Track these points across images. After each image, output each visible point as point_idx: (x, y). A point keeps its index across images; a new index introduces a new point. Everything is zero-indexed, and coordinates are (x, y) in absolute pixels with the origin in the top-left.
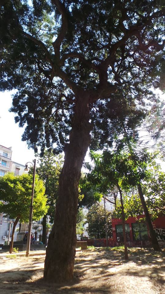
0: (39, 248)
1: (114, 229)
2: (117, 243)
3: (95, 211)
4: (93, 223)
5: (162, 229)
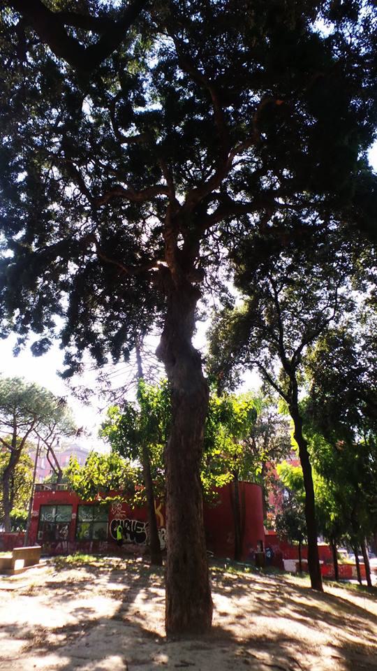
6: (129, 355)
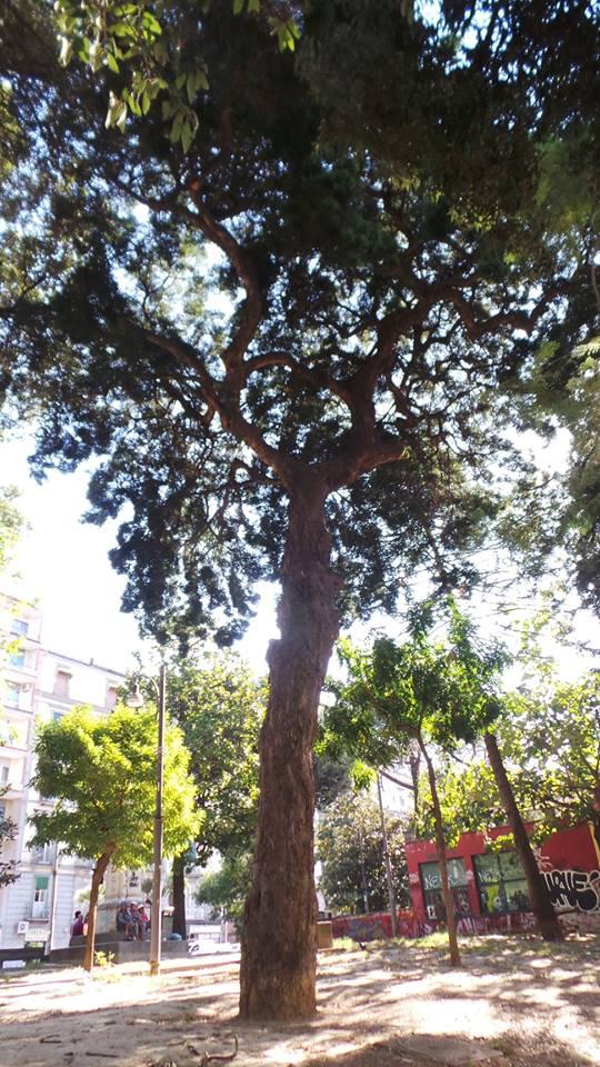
0: (171, 953)
1: (414, 878)
2: (427, 926)
3: (346, 815)
4: (341, 858)
5: (572, 873)
6: (393, 604)
